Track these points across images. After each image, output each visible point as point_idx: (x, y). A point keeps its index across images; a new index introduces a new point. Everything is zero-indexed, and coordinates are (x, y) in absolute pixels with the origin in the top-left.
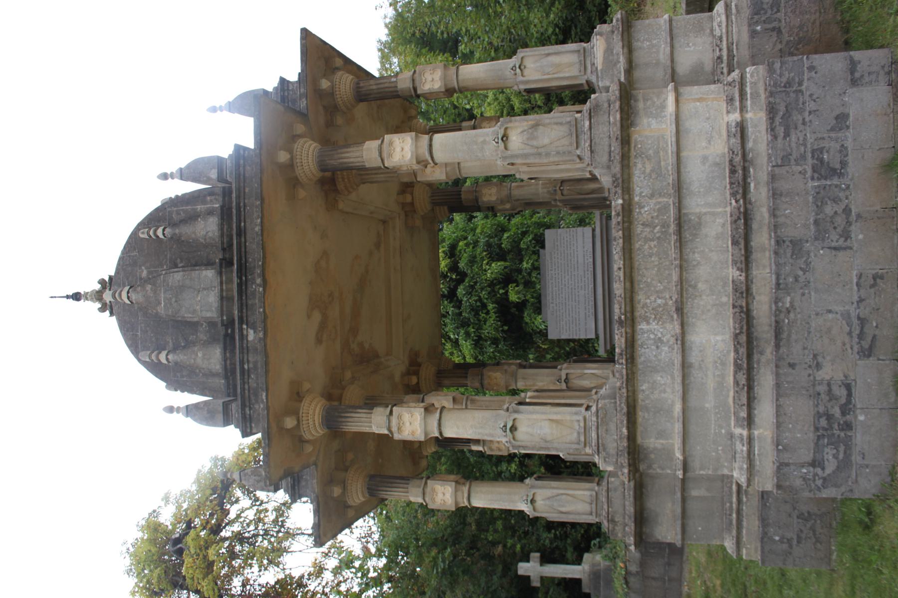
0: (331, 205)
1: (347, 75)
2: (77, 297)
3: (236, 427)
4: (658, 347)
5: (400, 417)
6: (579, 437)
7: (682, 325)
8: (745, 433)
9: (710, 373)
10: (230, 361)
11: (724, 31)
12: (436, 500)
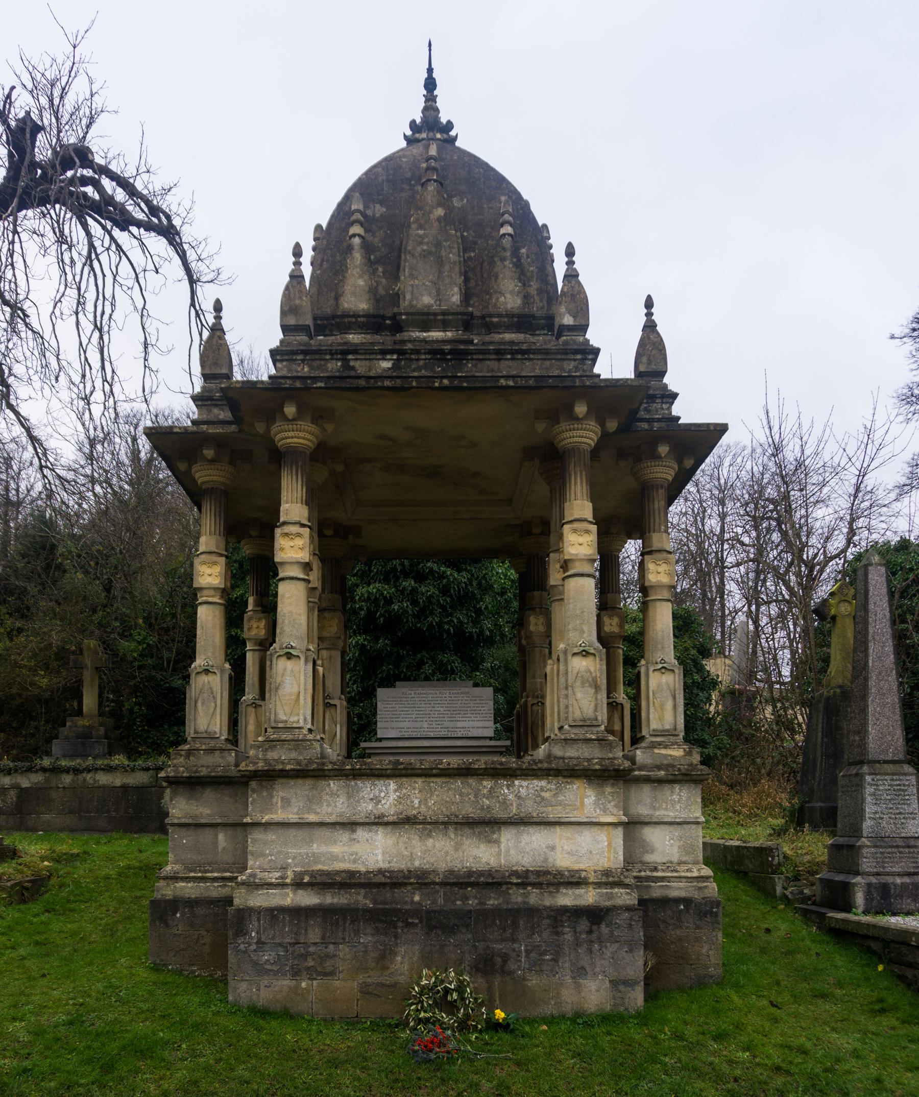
0: (529, 453)
1: (673, 474)
2: (430, 84)
3: (282, 342)
4: (372, 799)
5: (299, 535)
6: (282, 722)
7: (393, 823)
8: (288, 881)
9: (346, 848)
10: (354, 323)
11: (683, 874)
12: (204, 566)
